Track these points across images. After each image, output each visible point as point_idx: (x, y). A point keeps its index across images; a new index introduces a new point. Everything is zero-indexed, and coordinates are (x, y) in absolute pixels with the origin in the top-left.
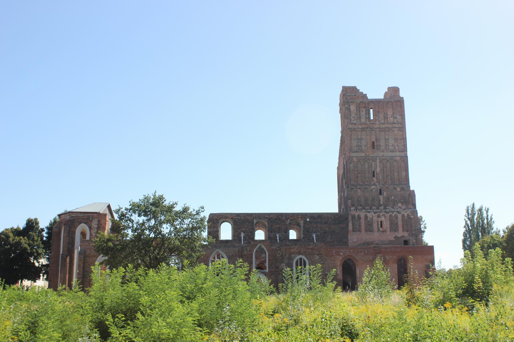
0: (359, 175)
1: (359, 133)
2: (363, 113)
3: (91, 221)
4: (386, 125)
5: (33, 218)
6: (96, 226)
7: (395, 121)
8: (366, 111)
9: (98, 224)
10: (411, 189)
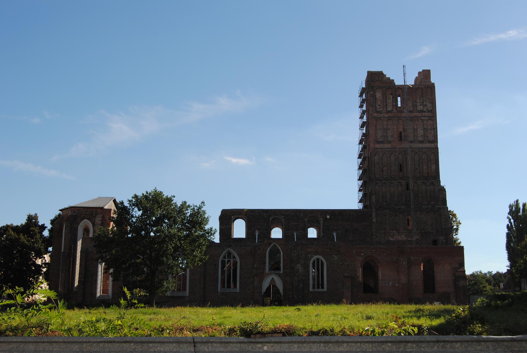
0: (385, 168)
1: (385, 123)
2: (390, 101)
3: (95, 217)
4: (415, 114)
5: (33, 214)
6: (100, 222)
7: (425, 110)
8: (393, 98)
9: (102, 221)
10: (442, 184)
